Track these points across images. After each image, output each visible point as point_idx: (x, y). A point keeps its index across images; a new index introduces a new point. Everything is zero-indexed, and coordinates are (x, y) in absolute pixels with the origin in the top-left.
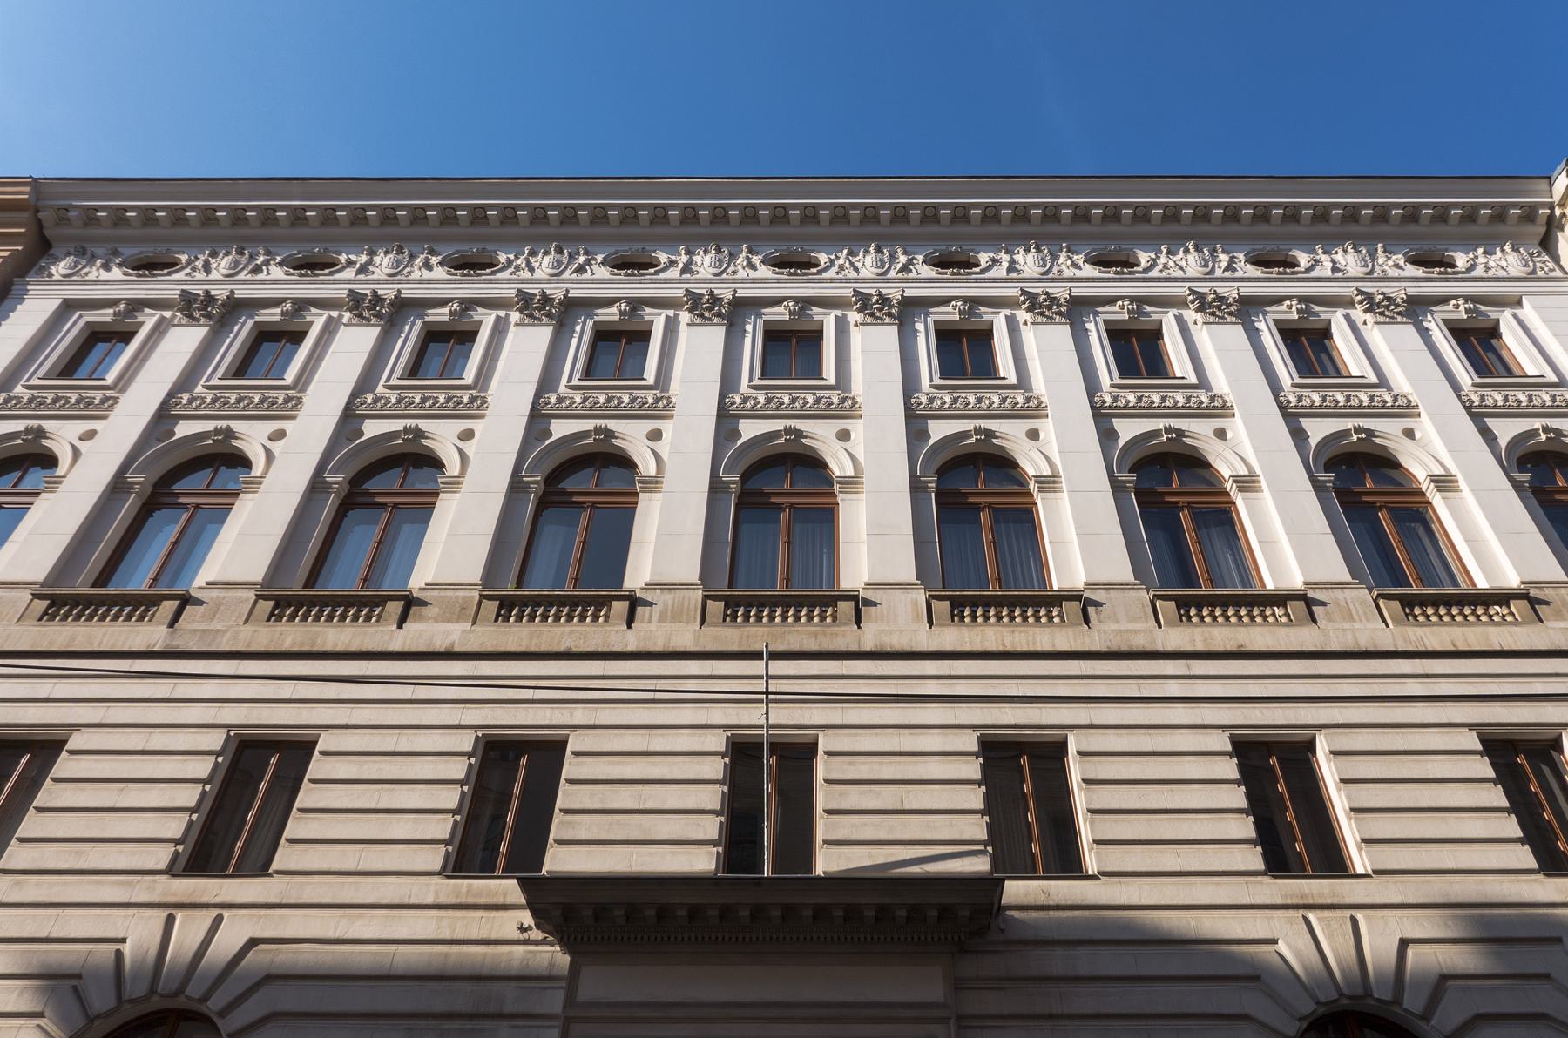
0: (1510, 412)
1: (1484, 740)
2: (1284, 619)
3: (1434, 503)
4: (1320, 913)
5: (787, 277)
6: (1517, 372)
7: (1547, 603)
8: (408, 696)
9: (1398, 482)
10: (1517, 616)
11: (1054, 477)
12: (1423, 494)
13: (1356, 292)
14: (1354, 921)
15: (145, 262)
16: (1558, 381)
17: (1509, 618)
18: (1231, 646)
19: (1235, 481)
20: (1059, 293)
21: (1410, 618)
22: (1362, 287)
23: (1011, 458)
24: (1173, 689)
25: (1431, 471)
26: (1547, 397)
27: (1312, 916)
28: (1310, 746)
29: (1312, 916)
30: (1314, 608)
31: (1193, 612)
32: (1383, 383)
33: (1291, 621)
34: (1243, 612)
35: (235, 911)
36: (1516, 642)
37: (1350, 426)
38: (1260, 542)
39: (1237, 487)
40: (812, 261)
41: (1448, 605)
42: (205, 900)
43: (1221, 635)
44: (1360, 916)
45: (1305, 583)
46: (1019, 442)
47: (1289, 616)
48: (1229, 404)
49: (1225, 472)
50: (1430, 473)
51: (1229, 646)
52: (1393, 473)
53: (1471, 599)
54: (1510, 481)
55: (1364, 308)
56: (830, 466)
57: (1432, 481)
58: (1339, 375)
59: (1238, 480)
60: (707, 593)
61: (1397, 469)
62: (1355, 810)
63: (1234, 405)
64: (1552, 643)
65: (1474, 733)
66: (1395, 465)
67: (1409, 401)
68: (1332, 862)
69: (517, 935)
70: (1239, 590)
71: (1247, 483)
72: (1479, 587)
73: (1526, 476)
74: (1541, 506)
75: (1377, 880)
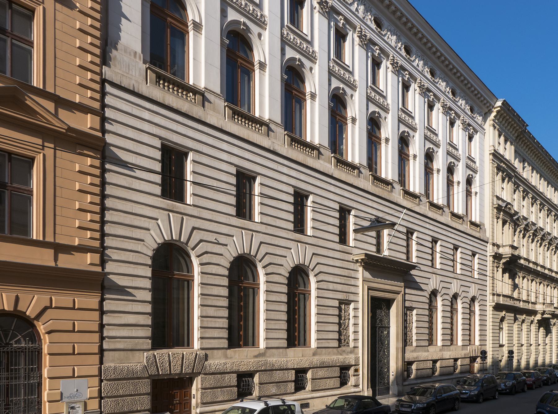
0: (294, 47)
1: (162, 145)
2: (193, 101)
3: (307, 101)
4: (187, 217)
5: (432, 81)
6: (340, 58)
7: (273, 132)
8: (130, 111)
9: (248, 56)
10: (263, 132)
11: (265, 64)
12: (347, 120)
13: (359, 27)
14: (183, 219)
15: (379, 22)
16: (258, 3)
17: (260, 131)
18: (301, 160)
19: (193, 23)
20: (368, 33)
21: (157, 83)
22: (362, 25)
23: (251, 46)
24: (225, 146)
25: (195, 19)
26: (305, 46)
27: (171, 214)
28: (186, 155)
29: (171, 214)
30: (270, 132)
31: (161, 82)
32: (311, 43)
33: (196, 102)
34: (304, 149)
35: (257, 234)
36: (173, 104)
37: (242, 20)
38: (194, 59)
39: (193, 27)
40: (409, 51)
41: (179, 87)
42: (438, 273)
43: (172, 99)
44: (185, 217)
45: (205, 88)
46: (307, 69)
47: (195, 100)
48: (356, 86)
49: (190, 17)
50: (194, 19)
51: (211, 122)
52: (300, 83)
53: (192, 90)
54: (221, 40)
55: (391, 62)
56: (188, 11)
57: (311, 94)
58: (298, 28)
59: (194, 23)
60: (150, 66)
61: (251, 51)
62: (313, 219)
63: (318, 59)
64: (273, 149)
65: (160, 141)
66: (251, 50)
67: (265, 21)
68: (180, 197)
69: (352, 260)
70: (245, 111)
71: (197, 26)
72: (348, 160)
73: (286, 77)
74: (227, 57)
75: (440, 270)
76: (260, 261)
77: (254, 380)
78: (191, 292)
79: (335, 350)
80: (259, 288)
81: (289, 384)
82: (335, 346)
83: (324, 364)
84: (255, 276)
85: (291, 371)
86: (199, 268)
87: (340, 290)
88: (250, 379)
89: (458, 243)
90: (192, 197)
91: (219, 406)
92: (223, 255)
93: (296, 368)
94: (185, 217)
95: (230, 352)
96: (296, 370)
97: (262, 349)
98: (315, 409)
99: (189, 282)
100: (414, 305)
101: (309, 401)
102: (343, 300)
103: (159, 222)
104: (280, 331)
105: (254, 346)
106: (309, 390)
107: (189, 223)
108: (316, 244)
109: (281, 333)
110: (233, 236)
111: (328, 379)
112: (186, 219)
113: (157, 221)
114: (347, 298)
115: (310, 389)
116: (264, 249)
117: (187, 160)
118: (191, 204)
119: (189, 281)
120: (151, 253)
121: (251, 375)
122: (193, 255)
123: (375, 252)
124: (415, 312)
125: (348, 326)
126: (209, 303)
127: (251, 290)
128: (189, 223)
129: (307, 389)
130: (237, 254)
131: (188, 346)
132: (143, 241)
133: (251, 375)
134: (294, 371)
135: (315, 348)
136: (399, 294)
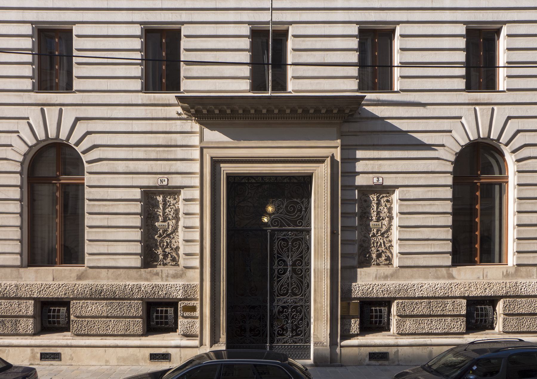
42: (493, 101)
44: (45, 108)
75: (508, 93)
76: (507, 145)
77: (497, 308)
78: (504, 198)
79: (133, 272)
80: (508, 182)
81: (23, 321)
82: (137, 266)
83: (103, 294)
84: (502, 168)
85: (25, 301)
86: (516, 166)
87: (147, 171)
88: (489, 308)
89: (481, 15)
90: (505, 81)
91: (450, 339)
92: (445, 145)
93: (468, 296)
94: (45, 108)
95: (455, 271)
96: (362, 300)
97: (510, 267)
98: (73, 364)
99: (502, 186)
100: (389, 181)
101: (170, 351)
102: (156, 187)
103: (463, 120)
104: (8, 242)
105: (501, 263)
106: (499, 332)
107: (501, 114)
108: (84, 103)
109: (9, 244)
110: (460, 118)
111: (112, 320)
112: (480, 109)
113: (28, 121)
114: (165, 183)
115: (501, 329)
116: (512, 126)
117: (499, 38)
118: (505, 90)
119: (501, 184)
120: (453, 158)
121: (493, 301)
122: (506, 151)
123: (249, 92)
124: (396, 196)
125: (389, 229)
126: (96, 210)
127: (497, 187)
128: (501, 114)
129: (496, 329)
130: (467, 141)
131: (499, 263)
132: (11, 146)
133: (493, 301)
134: (464, 301)
135: (514, 266)
136: (322, 162)
